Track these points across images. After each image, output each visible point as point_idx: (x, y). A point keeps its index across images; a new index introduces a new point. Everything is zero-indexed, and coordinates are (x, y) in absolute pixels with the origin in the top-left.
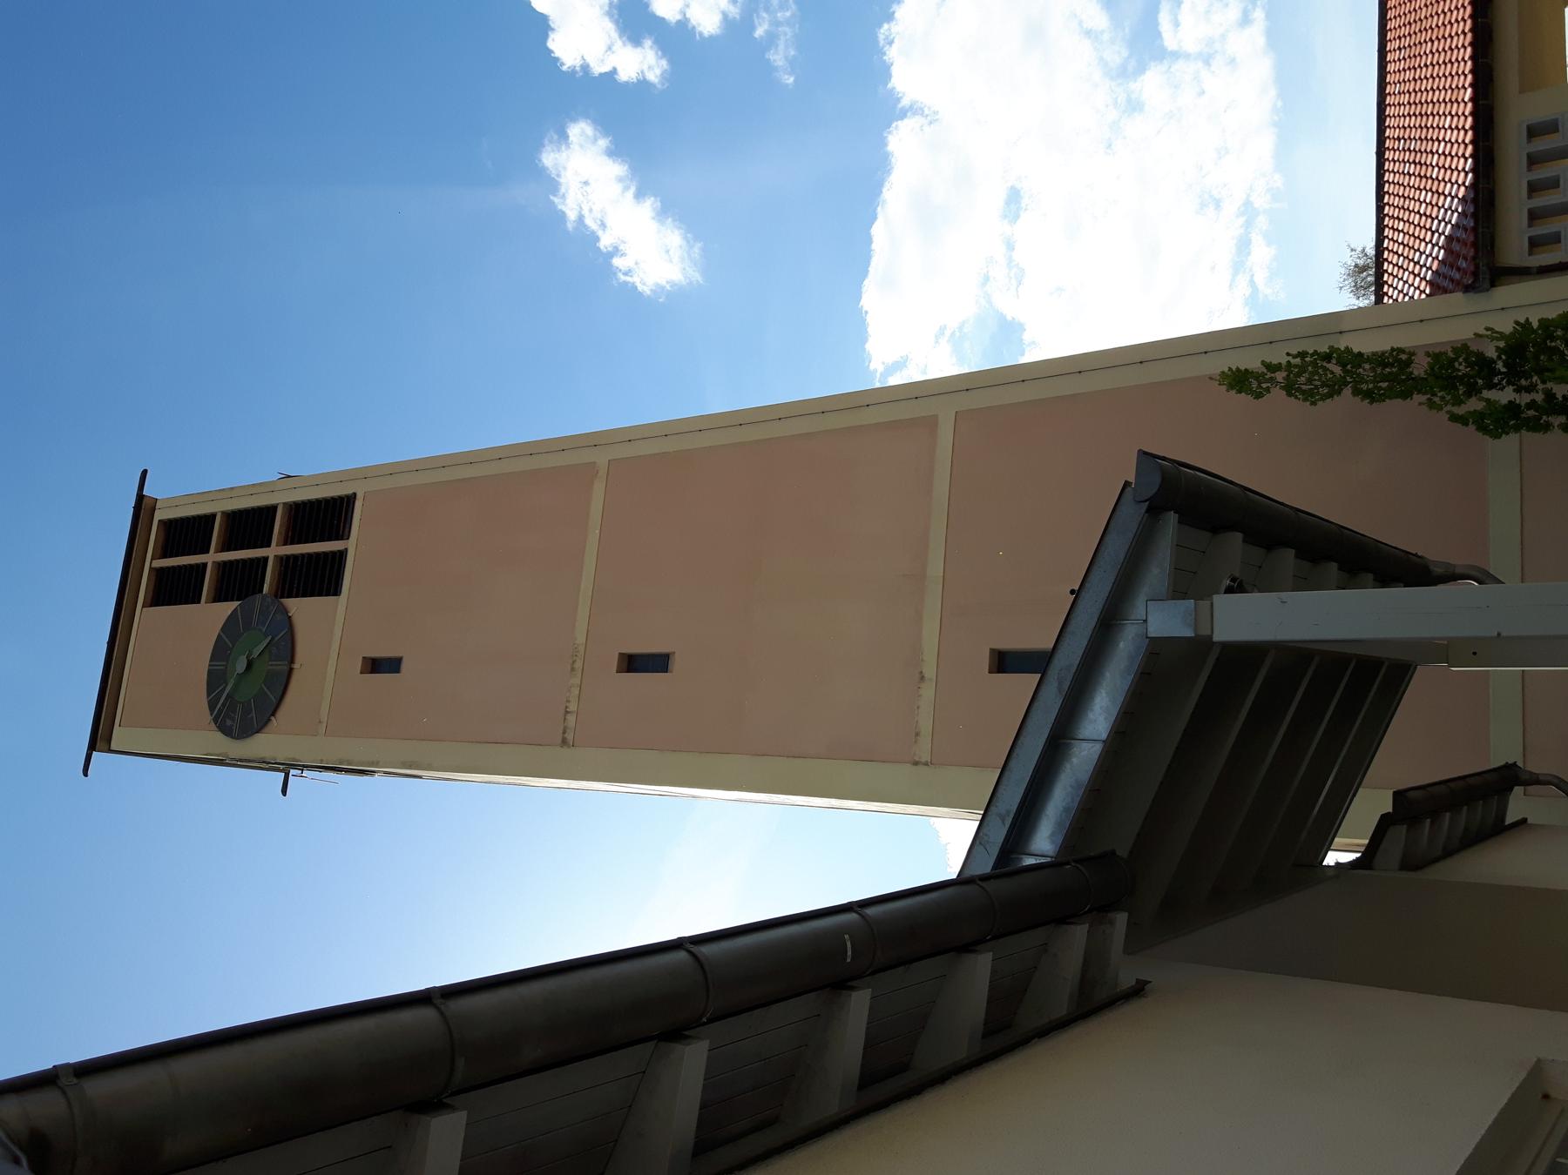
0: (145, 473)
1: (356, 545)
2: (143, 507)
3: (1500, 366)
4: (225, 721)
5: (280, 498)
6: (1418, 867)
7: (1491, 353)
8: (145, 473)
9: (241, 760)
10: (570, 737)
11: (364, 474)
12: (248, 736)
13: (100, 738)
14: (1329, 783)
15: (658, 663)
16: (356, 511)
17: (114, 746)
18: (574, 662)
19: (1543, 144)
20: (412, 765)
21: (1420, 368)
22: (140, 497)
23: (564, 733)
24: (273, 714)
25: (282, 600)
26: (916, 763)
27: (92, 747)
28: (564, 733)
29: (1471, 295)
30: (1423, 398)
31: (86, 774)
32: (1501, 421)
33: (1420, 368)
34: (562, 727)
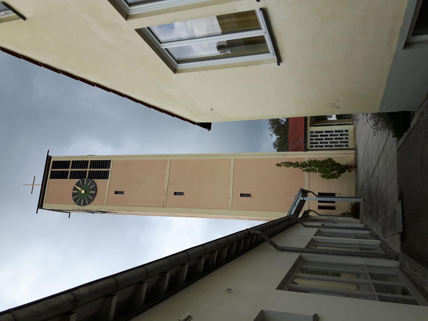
0: (49, 150)
1: (111, 170)
2: (49, 158)
3: (308, 164)
4: (79, 203)
5: (89, 159)
6: (306, 218)
7: (307, 163)
8: (49, 150)
9: (82, 210)
10: (165, 205)
11: (113, 156)
12: (85, 205)
13: (40, 206)
14: (90, 197)
15: (182, 194)
16: (111, 163)
17: (43, 207)
18: (165, 193)
19: (312, 134)
20: (130, 212)
21: (300, 164)
22: (48, 156)
23: (164, 205)
24: (92, 202)
25: (93, 180)
26: (229, 210)
27: (38, 208)
28: (164, 205)
29: (303, 152)
30: (299, 167)
31: (37, 213)
32: (308, 171)
33: (300, 164)
34: (163, 204)
